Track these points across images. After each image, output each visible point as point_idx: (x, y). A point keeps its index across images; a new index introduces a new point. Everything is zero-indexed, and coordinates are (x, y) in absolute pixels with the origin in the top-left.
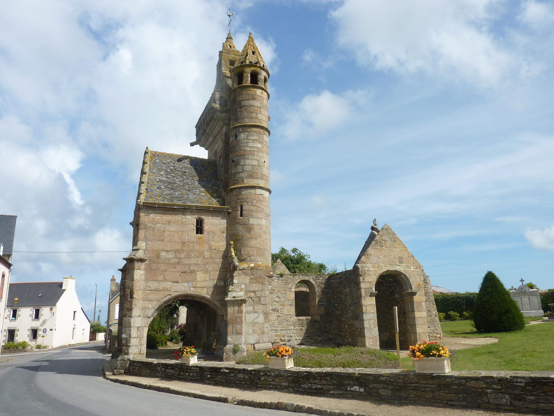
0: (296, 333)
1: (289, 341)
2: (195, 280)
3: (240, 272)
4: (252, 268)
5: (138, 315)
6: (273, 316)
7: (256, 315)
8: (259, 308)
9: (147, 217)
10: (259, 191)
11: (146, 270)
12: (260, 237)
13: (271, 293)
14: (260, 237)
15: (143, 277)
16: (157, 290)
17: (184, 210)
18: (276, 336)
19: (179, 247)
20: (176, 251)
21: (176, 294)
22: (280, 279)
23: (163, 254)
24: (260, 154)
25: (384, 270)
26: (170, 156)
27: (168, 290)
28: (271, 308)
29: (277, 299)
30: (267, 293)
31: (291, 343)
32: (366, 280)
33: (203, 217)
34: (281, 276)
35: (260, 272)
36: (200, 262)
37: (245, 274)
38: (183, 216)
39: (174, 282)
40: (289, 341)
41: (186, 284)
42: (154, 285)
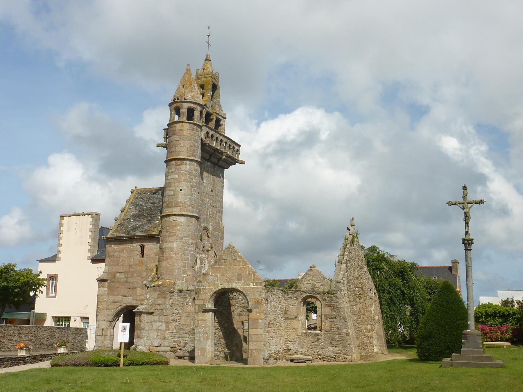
0: (190, 341)
1: (184, 347)
2: (136, 294)
3: (152, 288)
4: (160, 286)
5: (103, 319)
6: (172, 326)
7: (160, 324)
8: (163, 318)
9: (110, 248)
10: (172, 218)
11: (108, 287)
12: (170, 258)
13: (171, 306)
14: (170, 258)
15: (106, 292)
16: (113, 302)
17: (130, 240)
18: (174, 341)
19: (127, 269)
20: (126, 273)
21: (125, 305)
22: (180, 294)
23: (118, 275)
24: (176, 184)
25: (220, 288)
26: (149, 190)
27: (120, 302)
28: (171, 318)
29: (176, 312)
30: (168, 306)
31: (186, 348)
32: (200, 298)
33: (144, 244)
34: (181, 291)
35: (164, 289)
36: (139, 279)
37: (155, 290)
38: (131, 245)
39: (123, 296)
40: (184, 347)
41: (131, 298)
42: (112, 298)
